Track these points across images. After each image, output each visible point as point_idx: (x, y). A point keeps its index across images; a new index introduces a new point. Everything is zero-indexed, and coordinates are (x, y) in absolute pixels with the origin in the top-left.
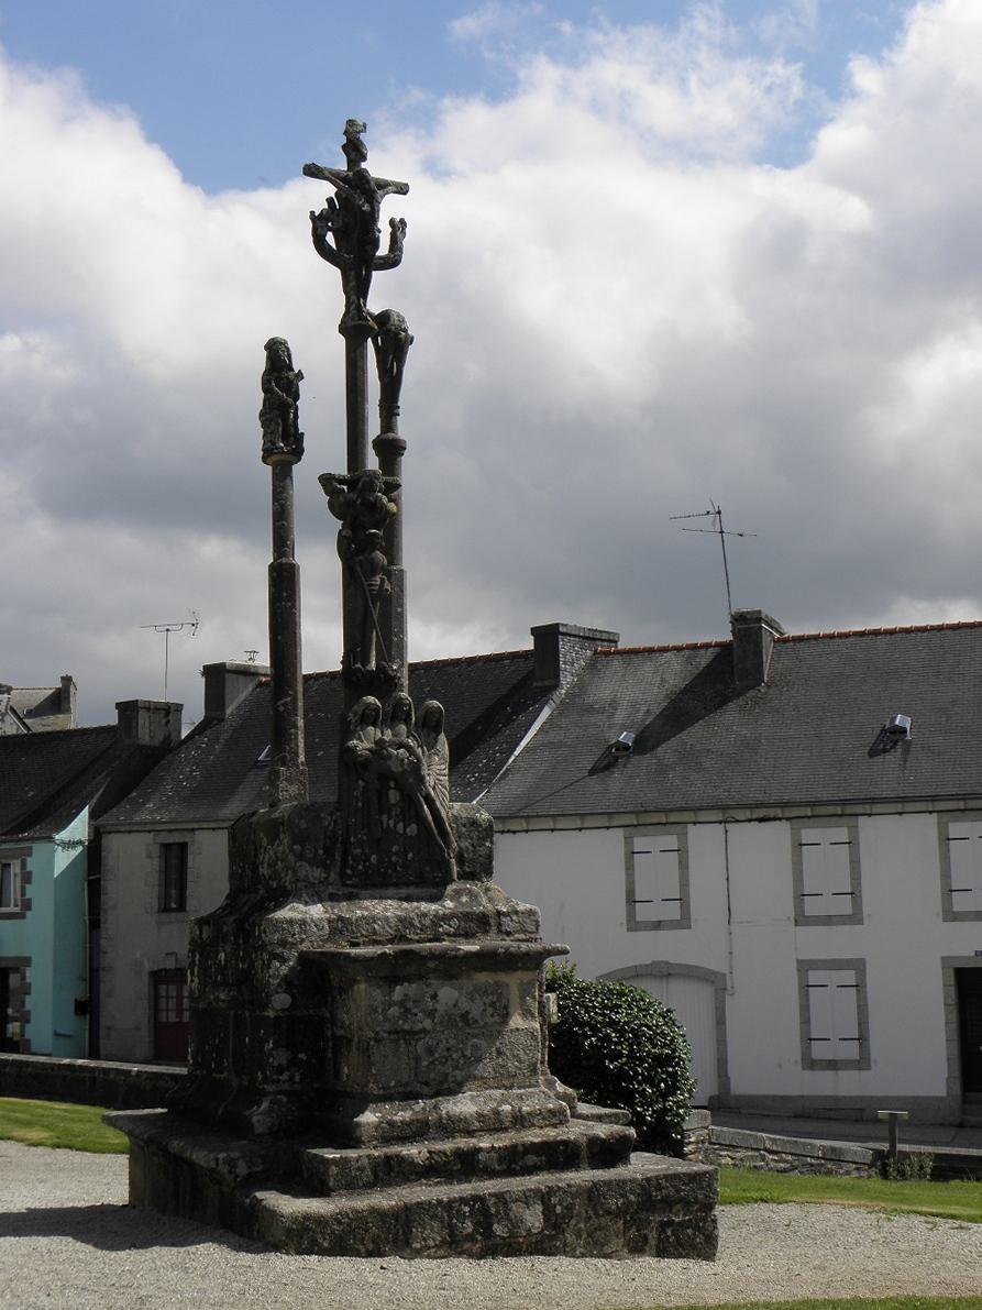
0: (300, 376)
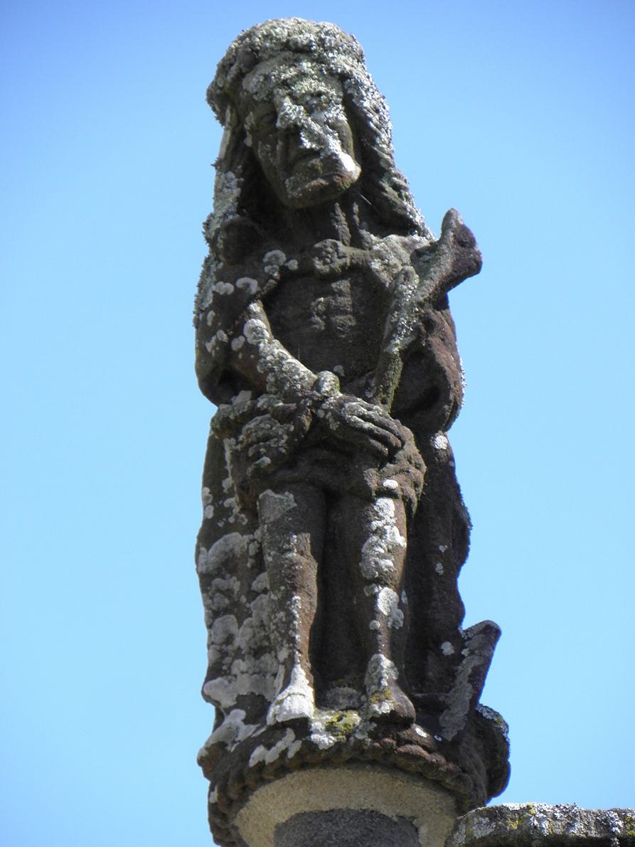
0: (461, 257)
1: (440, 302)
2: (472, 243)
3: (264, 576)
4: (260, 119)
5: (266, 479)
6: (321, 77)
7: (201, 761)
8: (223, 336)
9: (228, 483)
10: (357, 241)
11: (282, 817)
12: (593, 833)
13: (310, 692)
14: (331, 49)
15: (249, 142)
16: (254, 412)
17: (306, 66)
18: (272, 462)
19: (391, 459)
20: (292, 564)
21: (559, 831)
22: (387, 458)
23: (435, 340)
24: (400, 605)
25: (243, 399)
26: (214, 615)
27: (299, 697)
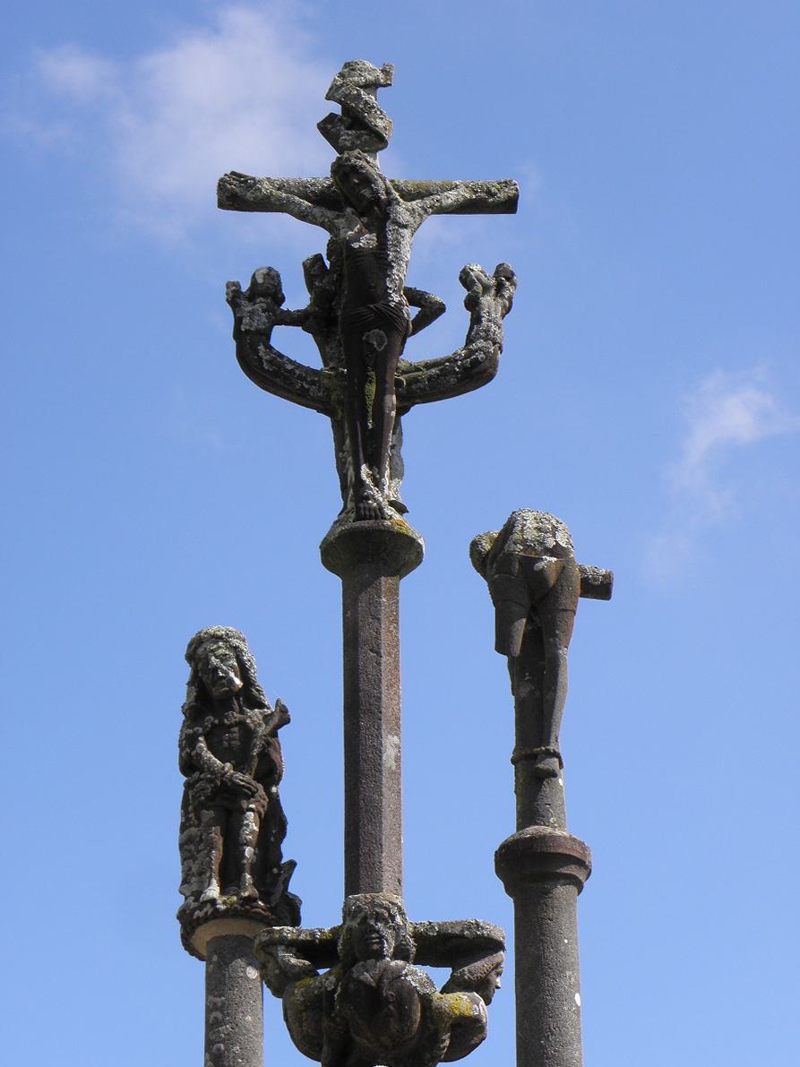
0: (283, 718)
1: (274, 734)
2: (287, 711)
3: (202, 844)
4: (203, 665)
5: (202, 806)
6: (227, 648)
7: (178, 918)
8: (188, 750)
9: (190, 808)
10: (242, 712)
11: (208, 938)
12: (308, 938)
13: (218, 889)
14: (231, 637)
15: (200, 675)
16: (199, 780)
17: (221, 644)
18: (519, 657)
19: (253, 796)
20: (212, 838)
21: (294, 937)
22: (251, 795)
23: (271, 750)
24: (255, 854)
25: (196, 775)
26: (184, 860)
27: (214, 891)
